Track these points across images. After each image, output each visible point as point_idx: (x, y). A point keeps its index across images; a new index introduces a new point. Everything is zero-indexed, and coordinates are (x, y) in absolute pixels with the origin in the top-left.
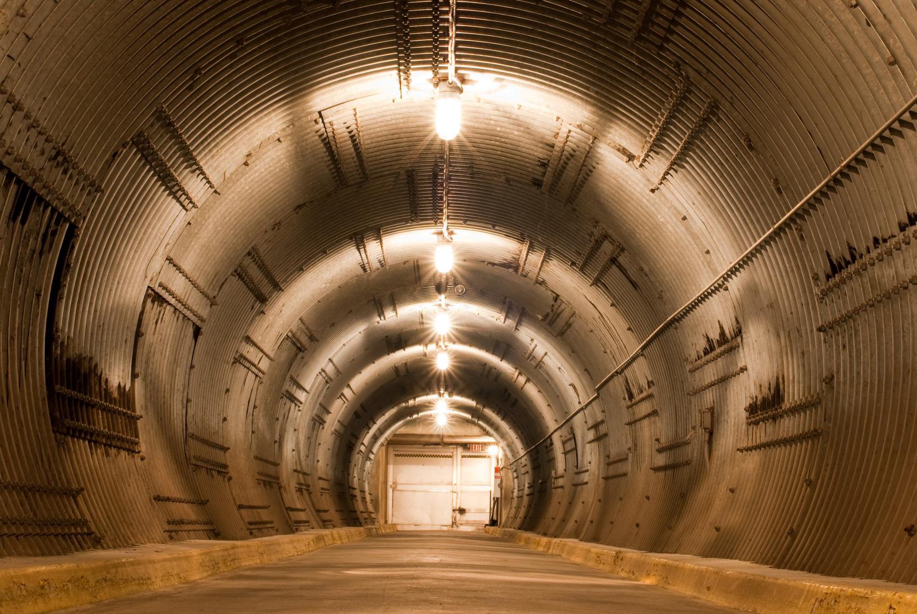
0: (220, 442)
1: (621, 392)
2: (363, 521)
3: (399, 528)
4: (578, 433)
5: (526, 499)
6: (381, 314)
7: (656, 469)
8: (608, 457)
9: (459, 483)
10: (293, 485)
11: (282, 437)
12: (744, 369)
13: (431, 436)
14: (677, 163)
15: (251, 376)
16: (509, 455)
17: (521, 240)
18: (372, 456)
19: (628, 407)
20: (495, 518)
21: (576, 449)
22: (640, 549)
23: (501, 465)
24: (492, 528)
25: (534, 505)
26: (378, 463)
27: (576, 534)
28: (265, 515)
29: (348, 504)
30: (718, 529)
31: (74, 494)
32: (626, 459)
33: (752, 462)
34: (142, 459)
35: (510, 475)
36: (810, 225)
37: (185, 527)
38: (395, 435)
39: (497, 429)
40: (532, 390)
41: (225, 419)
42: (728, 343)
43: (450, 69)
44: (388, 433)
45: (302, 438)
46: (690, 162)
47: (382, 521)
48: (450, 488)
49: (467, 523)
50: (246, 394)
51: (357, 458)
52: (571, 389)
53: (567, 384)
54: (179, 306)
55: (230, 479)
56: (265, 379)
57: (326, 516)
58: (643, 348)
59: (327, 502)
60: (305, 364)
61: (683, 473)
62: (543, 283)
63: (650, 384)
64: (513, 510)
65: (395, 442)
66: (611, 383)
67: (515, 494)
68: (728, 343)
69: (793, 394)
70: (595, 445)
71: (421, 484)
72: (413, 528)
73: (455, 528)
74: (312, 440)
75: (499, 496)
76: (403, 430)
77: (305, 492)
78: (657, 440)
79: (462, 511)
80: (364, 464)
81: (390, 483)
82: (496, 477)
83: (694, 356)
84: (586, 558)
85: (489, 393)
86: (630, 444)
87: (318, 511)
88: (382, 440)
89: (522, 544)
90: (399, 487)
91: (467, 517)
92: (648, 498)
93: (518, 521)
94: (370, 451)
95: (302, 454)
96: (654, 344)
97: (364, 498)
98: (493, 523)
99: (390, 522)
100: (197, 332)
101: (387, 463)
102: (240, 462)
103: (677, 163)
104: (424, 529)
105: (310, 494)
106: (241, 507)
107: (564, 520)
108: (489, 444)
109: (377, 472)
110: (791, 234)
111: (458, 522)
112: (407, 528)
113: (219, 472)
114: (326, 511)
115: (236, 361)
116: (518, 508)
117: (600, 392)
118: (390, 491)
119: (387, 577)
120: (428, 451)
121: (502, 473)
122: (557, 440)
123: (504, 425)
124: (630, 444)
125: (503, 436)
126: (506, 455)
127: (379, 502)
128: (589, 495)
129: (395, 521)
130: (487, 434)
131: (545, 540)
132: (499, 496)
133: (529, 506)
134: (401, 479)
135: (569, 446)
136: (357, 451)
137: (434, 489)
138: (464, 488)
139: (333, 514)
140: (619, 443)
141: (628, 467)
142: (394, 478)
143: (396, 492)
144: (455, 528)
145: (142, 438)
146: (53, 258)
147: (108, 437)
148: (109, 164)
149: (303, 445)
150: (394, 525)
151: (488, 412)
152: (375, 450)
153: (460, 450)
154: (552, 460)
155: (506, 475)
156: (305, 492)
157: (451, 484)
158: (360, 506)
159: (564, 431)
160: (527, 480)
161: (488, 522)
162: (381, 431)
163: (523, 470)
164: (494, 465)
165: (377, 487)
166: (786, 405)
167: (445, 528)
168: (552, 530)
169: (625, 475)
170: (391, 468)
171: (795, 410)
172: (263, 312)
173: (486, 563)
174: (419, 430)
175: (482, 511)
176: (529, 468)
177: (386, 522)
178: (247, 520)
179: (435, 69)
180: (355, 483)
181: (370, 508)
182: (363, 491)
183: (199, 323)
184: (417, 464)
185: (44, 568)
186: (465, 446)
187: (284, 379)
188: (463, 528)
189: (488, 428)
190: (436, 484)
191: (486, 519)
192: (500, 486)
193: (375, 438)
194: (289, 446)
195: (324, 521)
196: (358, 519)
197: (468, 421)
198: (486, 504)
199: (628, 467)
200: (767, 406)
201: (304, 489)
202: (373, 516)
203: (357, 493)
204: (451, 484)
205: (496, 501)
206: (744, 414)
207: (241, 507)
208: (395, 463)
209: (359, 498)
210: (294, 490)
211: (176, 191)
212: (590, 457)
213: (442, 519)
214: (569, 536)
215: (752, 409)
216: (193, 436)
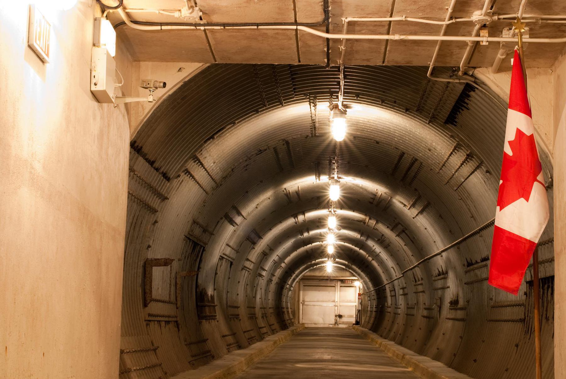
0: (236, 305)
1: (412, 276)
2: (288, 325)
3: (306, 326)
4: (396, 288)
5: (374, 313)
6: (302, 234)
7: (424, 317)
8: (408, 304)
9: (339, 301)
10: (260, 315)
11: (256, 294)
12: (449, 287)
13: (325, 276)
14: (421, 212)
15: (247, 272)
16: (366, 288)
17: (366, 215)
18: (292, 289)
19: (415, 285)
20: (358, 320)
21: (395, 296)
22: (415, 352)
23: (361, 292)
24: (357, 326)
25: (376, 316)
26: (295, 291)
27: (393, 339)
28: (253, 334)
29: (282, 316)
30: (438, 349)
31: (205, 341)
32: (414, 308)
33: (450, 324)
34: (218, 321)
35: (366, 298)
36: (461, 246)
37: (231, 346)
38: (304, 276)
39: (359, 275)
40: (375, 263)
41: (238, 294)
42: (443, 275)
43: (335, 176)
44: (301, 275)
45: (263, 291)
46: (425, 214)
47: (297, 322)
48: (334, 304)
49: (343, 323)
50: (244, 280)
51: (285, 291)
52: (392, 269)
53: (390, 266)
54: (228, 258)
55: (240, 320)
56: (251, 272)
57: (273, 327)
58: (419, 264)
59: (273, 320)
60: (267, 259)
61: (432, 322)
62: (377, 229)
63: (422, 279)
64: (368, 318)
65: (304, 279)
66: (408, 272)
67: (369, 309)
68: (443, 275)
69: (461, 303)
70: (403, 296)
71: (318, 301)
72: (313, 326)
73: (336, 326)
74: (267, 291)
75: (360, 309)
76: (309, 274)
77: (265, 317)
78: (425, 304)
79: (340, 316)
80: (288, 294)
81: (301, 301)
82: (359, 299)
83: (435, 275)
84: (393, 355)
85: (353, 259)
86: (415, 302)
87: (270, 326)
88: (297, 279)
89: (370, 340)
90: (306, 303)
91: (344, 319)
92: (420, 329)
93: (370, 325)
94: (291, 286)
95: (263, 298)
96: (422, 264)
97: (288, 312)
98: (357, 323)
99: (301, 322)
100: (231, 264)
101: (299, 290)
102: (243, 312)
103: (421, 212)
104: (319, 326)
105: (266, 317)
106: (244, 332)
107: (390, 331)
108: (355, 280)
109: (294, 296)
110: (456, 247)
111: (338, 322)
112: (310, 326)
113: (237, 318)
114: (273, 324)
115: (242, 269)
116: (370, 317)
117: (405, 274)
118: (301, 305)
119: (312, 369)
120: (322, 283)
121: (362, 297)
122: (387, 287)
123: (362, 274)
124: (415, 302)
125: (362, 278)
126: (364, 287)
127: (295, 313)
128: (401, 320)
129: (304, 322)
130: (354, 276)
131: (380, 340)
132: (360, 309)
133: (375, 318)
134: (307, 299)
135: (393, 293)
136: (285, 288)
137: (324, 304)
138: (342, 304)
139: (276, 326)
140: (412, 299)
141: (414, 312)
142: (303, 298)
143: (304, 306)
144: (336, 326)
145: (217, 314)
146: (198, 260)
147: (209, 316)
148: (216, 226)
149: (263, 296)
150: (303, 324)
151: (354, 267)
152: (293, 286)
153: (339, 283)
154: (386, 297)
155: (364, 298)
156: (265, 317)
157: (334, 301)
158: (286, 317)
159: (390, 285)
160: (375, 303)
161: (354, 322)
162: (297, 276)
163: (373, 298)
164: (358, 292)
165: (294, 304)
166: (459, 306)
167: (331, 326)
168: (384, 334)
169: (413, 315)
170: (301, 293)
171: (461, 309)
172: (254, 248)
173: (350, 359)
174: (317, 274)
175: (351, 316)
176: (375, 297)
177: (299, 322)
178: (247, 338)
179: (329, 175)
180: (284, 305)
181: (291, 317)
182: (288, 308)
183: (232, 260)
184: (315, 290)
185: (217, 372)
186: (342, 281)
187: (258, 268)
188: (341, 326)
189: (354, 273)
190: (326, 302)
191: (353, 320)
192: (361, 303)
193: (294, 280)
194: (258, 296)
195: (273, 330)
196: (286, 325)
197: (343, 269)
198: (353, 313)
199: (414, 312)
200: (454, 303)
201: (264, 316)
202: (293, 320)
203: (285, 310)
204: (334, 301)
205: (359, 311)
206: (449, 305)
207: (244, 332)
208: (304, 290)
209: (286, 313)
210: (260, 317)
211: (232, 222)
212: (401, 301)
213: (330, 320)
214: (391, 340)
215: (451, 303)
216: (230, 306)
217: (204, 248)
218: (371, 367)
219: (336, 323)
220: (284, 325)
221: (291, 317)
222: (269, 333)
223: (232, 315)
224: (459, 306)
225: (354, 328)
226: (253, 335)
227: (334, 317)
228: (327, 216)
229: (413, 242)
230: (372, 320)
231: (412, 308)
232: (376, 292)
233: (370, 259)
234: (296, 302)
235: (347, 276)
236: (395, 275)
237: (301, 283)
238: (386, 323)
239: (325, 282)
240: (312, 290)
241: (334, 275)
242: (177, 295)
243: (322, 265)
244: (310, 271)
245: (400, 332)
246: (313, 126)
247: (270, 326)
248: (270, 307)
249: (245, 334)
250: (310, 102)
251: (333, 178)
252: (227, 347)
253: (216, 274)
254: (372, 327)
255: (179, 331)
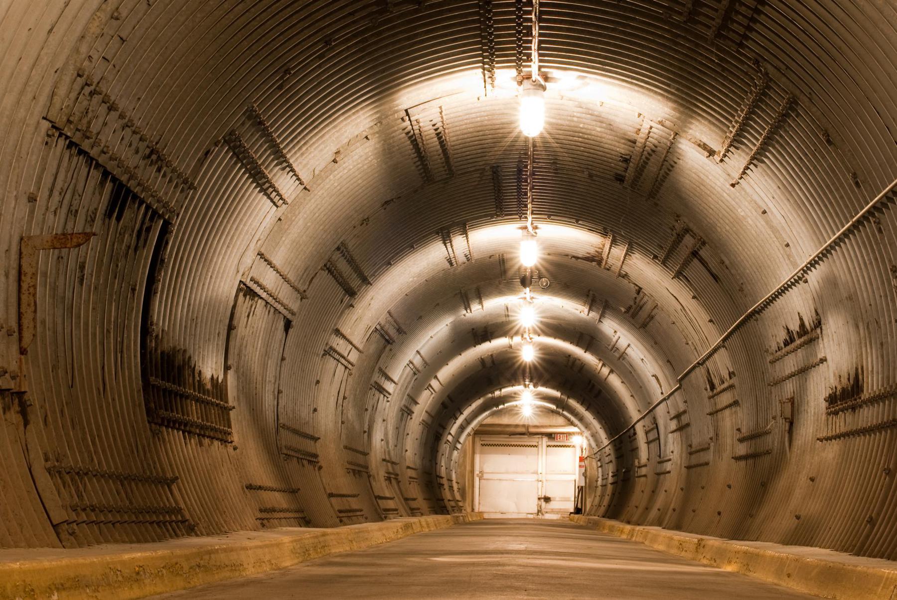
3: (486, 516)
4: (661, 423)
5: (610, 487)
6: (467, 307)
7: (738, 459)
8: (690, 446)
9: (544, 473)
10: (382, 474)
14: (756, 158)
17: (604, 234)
18: (459, 446)
19: (710, 398)
20: (579, 506)
21: (658, 438)
23: (585, 455)
24: (577, 516)
25: (617, 493)
27: (659, 523)
28: (354, 504)
29: (436, 492)
30: (798, 517)
31: (168, 482)
33: (831, 452)
34: (235, 449)
35: (594, 464)
39: (581, 419)
40: (615, 381)
41: (315, 410)
47: (469, 510)
48: (535, 477)
49: (553, 511)
51: (444, 448)
52: (653, 380)
53: (649, 375)
54: (270, 300)
55: (320, 468)
56: (354, 371)
57: (414, 504)
58: (724, 340)
59: (415, 491)
60: (393, 356)
62: (626, 276)
63: (731, 375)
64: (597, 499)
65: (482, 432)
66: (693, 375)
68: (807, 334)
69: (872, 385)
71: (507, 473)
73: (540, 516)
75: (583, 485)
76: (490, 421)
77: (393, 481)
78: (739, 430)
79: (547, 499)
80: (451, 454)
81: (477, 472)
82: (580, 466)
83: (774, 347)
85: (573, 383)
86: (712, 434)
87: (406, 499)
88: (469, 430)
89: (606, 531)
90: (485, 476)
91: (553, 505)
92: (729, 487)
93: (602, 509)
97: (451, 487)
98: (578, 511)
99: (476, 510)
100: (288, 325)
101: (474, 453)
102: (330, 452)
103: (756, 158)
106: (331, 495)
107: (647, 509)
108: (573, 433)
109: (464, 461)
111: (543, 510)
113: (310, 462)
114: (414, 499)
116: (602, 496)
117: (683, 382)
118: (477, 480)
120: (514, 440)
122: (639, 428)
123: (588, 416)
125: (587, 426)
126: (590, 445)
127: (466, 492)
129: (482, 509)
132: (583, 485)
133: (613, 494)
134: (487, 469)
135: (652, 436)
136: (444, 440)
137: (519, 478)
139: (421, 502)
140: (701, 432)
141: (709, 456)
142: (481, 467)
143: (482, 481)
144: (540, 516)
145: (235, 429)
149: (392, 435)
150: (481, 513)
151: (573, 402)
152: (462, 440)
153: (545, 439)
154: (635, 450)
155: (591, 464)
156: (393, 481)
157: (536, 473)
158: (447, 495)
159: (647, 421)
160: (611, 469)
161: (572, 510)
162: (468, 422)
163: (607, 460)
165: (464, 476)
166: (865, 395)
167: (531, 516)
168: (635, 518)
169: (707, 464)
170: (477, 458)
171: (874, 400)
172: (352, 306)
174: (505, 420)
175: (566, 500)
176: (612, 457)
177: (473, 510)
178: (337, 508)
179: (518, 67)
180: (443, 472)
182: (450, 480)
183: (289, 316)
184: (503, 453)
186: (550, 436)
188: (548, 516)
189: (572, 418)
190: (522, 473)
193: (462, 428)
195: (412, 509)
196: (445, 507)
197: (552, 411)
198: (570, 493)
199: (709, 456)
200: (847, 397)
201: (392, 477)
202: (461, 504)
203: (444, 481)
204: (536, 473)
205: (581, 489)
206: (824, 405)
207: (331, 495)
208: (482, 453)
209: (446, 487)
210: (382, 479)
211: (266, 187)
212: (673, 446)
213: (528, 507)
214: (651, 524)
216: (284, 426)
217: (167, 225)
218: (627, 564)
219: (539, 511)
220: (439, 506)
221: (458, 497)
222: (402, 511)
223: (289, 448)
224: (865, 395)
225: (571, 520)
226: (355, 507)
227: (537, 500)
228: (520, 345)
229: (715, 277)
230: (607, 499)
231: (703, 450)
232: (615, 446)
233: (605, 371)
234: (469, 474)
235: (558, 425)
236: (659, 391)
237: (477, 439)
238: (638, 497)
239: (520, 436)
240: (497, 453)
241: (536, 423)
242: (23, 310)
243: (514, 403)
244: (493, 414)
245: (672, 506)
246: (511, 347)
247: (406, 499)
248: (407, 464)
249: (332, 499)
250: (484, 69)
251: (529, 77)
252: (259, 515)
253: (231, 328)
254: (607, 511)
255: (26, 423)
